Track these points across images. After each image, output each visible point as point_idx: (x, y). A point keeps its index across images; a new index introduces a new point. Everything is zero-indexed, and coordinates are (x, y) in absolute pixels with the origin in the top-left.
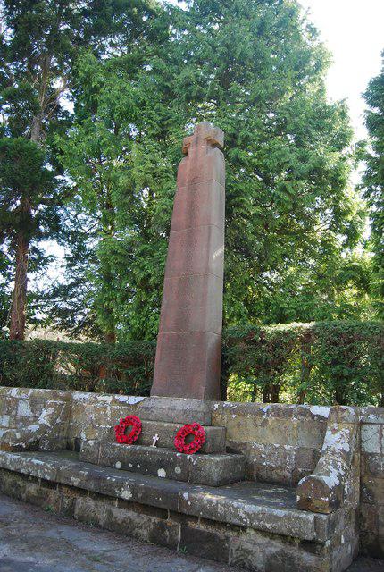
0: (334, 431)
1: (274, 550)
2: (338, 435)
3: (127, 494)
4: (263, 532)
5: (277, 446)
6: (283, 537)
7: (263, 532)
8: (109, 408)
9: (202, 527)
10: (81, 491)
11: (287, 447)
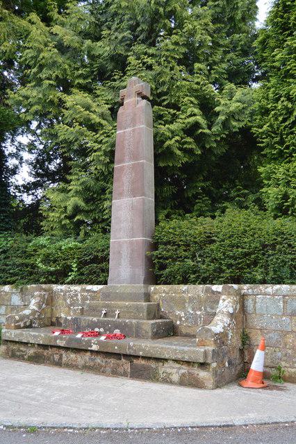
0: (224, 300)
1: (183, 371)
2: (226, 303)
3: (95, 348)
4: (176, 361)
5: (192, 312)
6: (188, 363)
7: (176, 361)
8: (79, 295)
9: (143, 362)
10: (66, 349)
11: (199, 313)
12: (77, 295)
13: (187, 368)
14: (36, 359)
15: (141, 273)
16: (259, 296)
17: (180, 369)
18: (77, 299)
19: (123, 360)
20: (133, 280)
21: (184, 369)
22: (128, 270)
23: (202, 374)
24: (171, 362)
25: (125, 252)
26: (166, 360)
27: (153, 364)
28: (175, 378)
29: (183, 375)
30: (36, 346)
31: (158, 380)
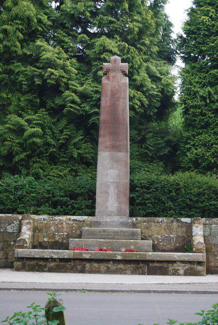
2: (199, 228)
3: (119, 258)
8: (64, 223)
11: (171, 236)
12: (62, 223)
13: (190, 265)
14: (204, 293)
15: (126, 208)
16: (213, 225)
17: (184, 266)
18: (63, 227)
19: (141, 265)
20: (120, 213)
21: (188, 266)
22: (116, 205)
23: (200, 268)
24: (179, 263)
25: (112, 191)
26: (175, 262)
27: (165, 265)
28: (182, 272)
29: (187, 269)
30: (57, 260)
31: (168, 275)
